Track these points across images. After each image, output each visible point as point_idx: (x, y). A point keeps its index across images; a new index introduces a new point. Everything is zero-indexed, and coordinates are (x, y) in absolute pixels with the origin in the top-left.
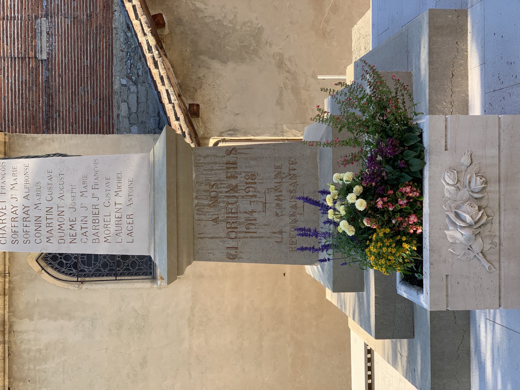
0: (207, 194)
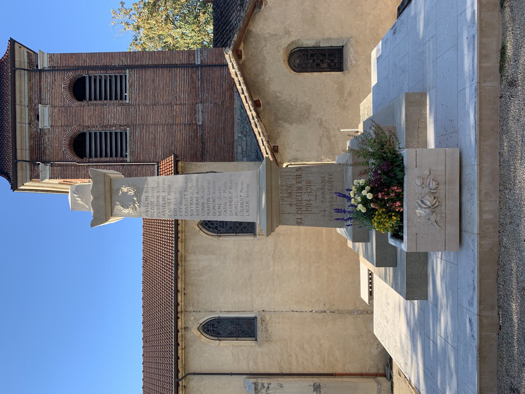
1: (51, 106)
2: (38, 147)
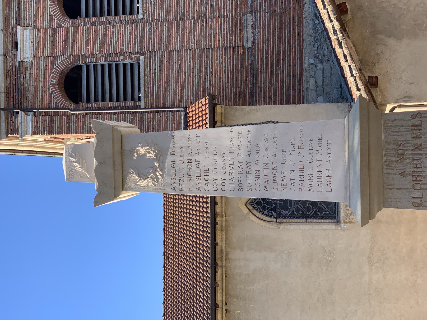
0: (394, 152)
1: (34, 28)
2: (17, 88)
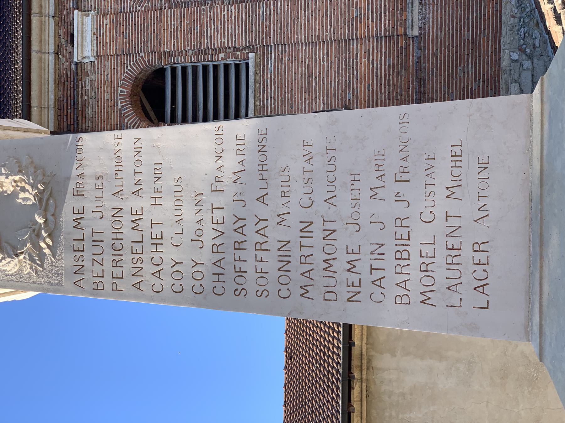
1: (98, 13)
2: (72, 101)
